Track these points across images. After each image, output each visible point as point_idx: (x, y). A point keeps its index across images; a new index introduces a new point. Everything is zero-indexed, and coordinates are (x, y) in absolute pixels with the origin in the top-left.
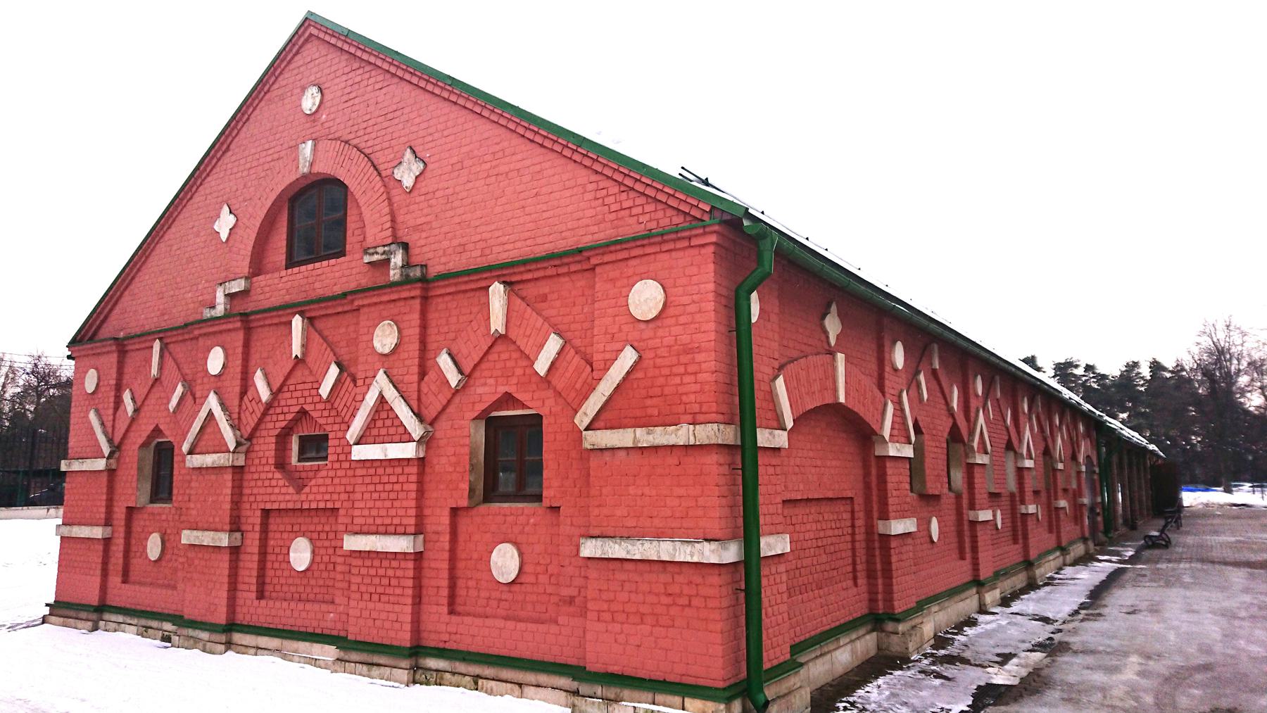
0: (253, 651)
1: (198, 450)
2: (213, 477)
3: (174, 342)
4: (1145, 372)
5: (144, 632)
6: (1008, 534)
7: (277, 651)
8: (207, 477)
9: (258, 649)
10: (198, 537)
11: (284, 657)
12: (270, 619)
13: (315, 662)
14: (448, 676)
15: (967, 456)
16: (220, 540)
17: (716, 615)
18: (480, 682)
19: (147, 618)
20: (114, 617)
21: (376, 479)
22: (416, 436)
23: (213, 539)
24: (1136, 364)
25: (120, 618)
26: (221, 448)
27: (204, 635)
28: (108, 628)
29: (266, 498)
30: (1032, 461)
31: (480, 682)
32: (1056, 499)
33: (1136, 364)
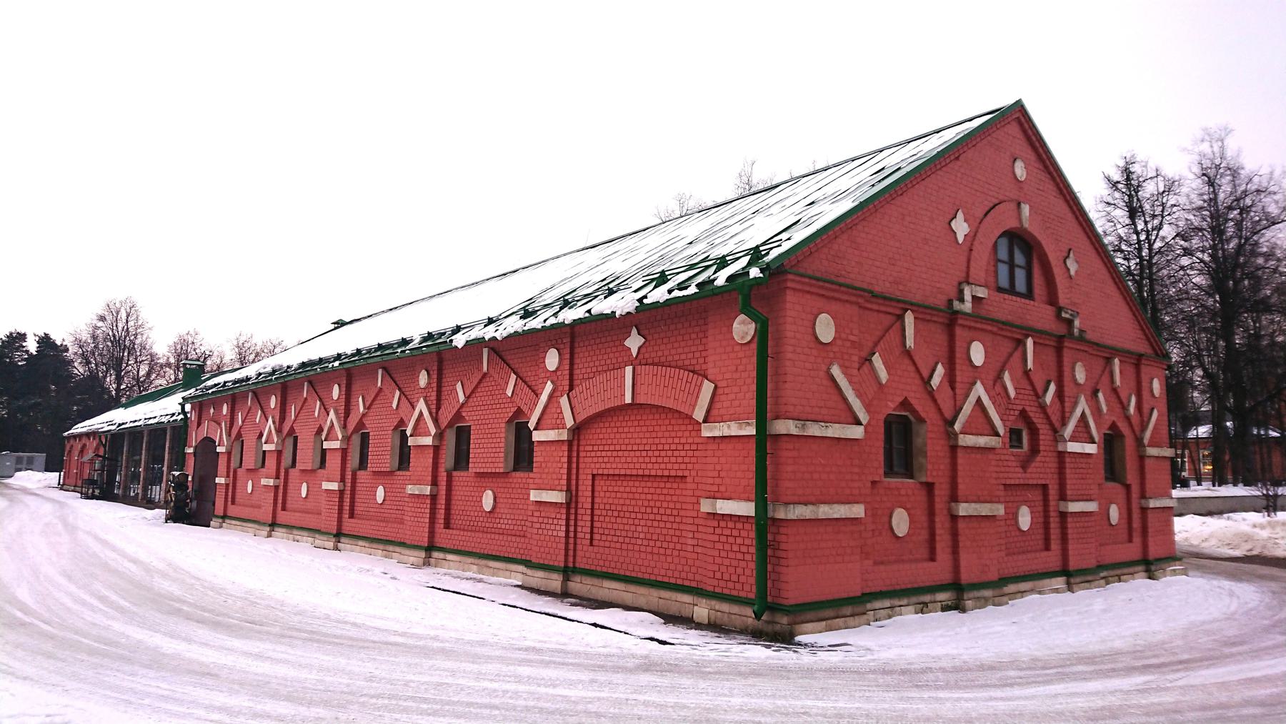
0: (1020, 595)
1: (541, 427)
2: (979, 456)
3: (794, 289)
4: (32, 346)
5: (923, 608)
6: (358, 508)
7: (1032, 591)
8: (973, 455)
9: (1022, 593)
10: (976, 509)
11: (1040, 593)
12: (1016, 570)
13: (1057, 591)
14: (1110, 579)
15: (1056, 441)
16: (998, 510)
17: (1038, 537)
18: (1122, 577)
19: (1119, 568)
20: (878, 604)
21: (647, 460)
22: (864, 422)
23: (991, 509)
24: (22, 337)
25: (887, 603)
26: (559, 425)
27: (987, 593)
28: (878, 617)
29: (1006, 475)
30: (1095, 446)
31: (1122, 577)
32: (227, 485)
33: (22, 337)
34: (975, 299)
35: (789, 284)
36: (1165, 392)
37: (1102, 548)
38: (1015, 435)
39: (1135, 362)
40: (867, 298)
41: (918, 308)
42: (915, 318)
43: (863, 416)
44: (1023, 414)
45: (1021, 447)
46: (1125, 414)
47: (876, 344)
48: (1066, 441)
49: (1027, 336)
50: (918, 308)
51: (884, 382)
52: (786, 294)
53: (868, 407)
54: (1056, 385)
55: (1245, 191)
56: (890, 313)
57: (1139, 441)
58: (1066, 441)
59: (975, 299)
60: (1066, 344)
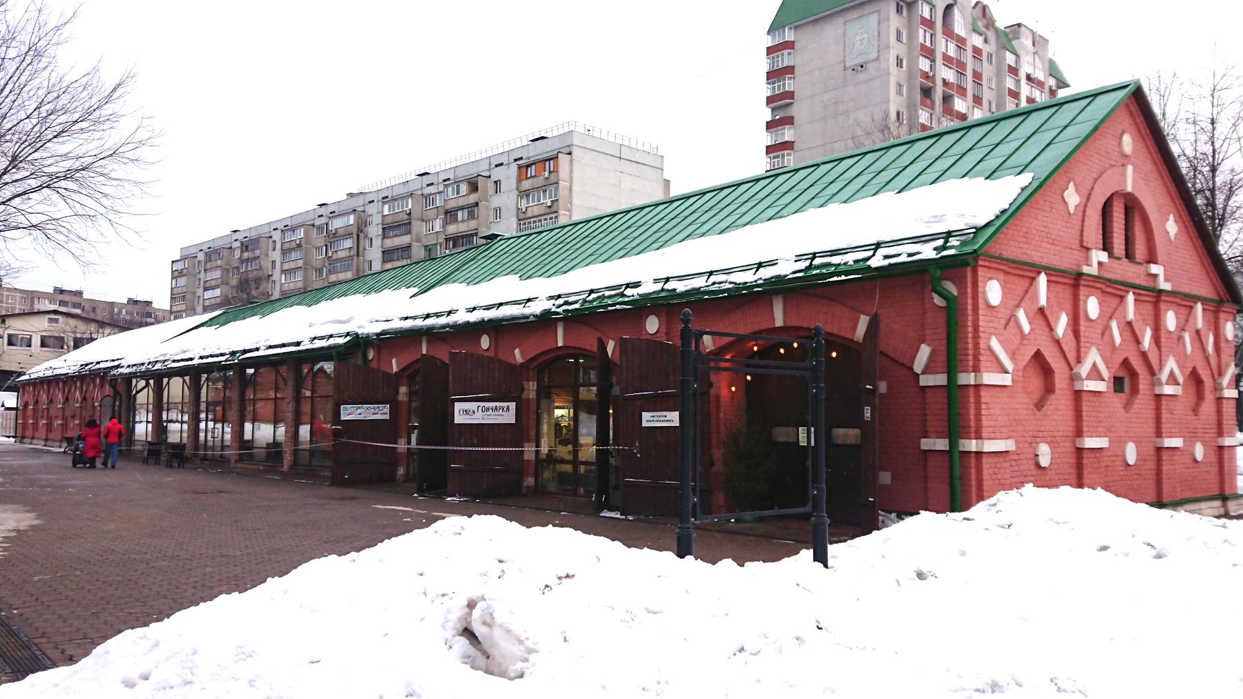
15: (1153, 385)
34: (1100, 264)
35: (1082, 282)
36: (1162, 318)
37: (522, 638)
38: (1118, 383)
39: (1072, 282)
40: (1029, 271)
41: (1051, 271)
42: (1048, 281)
43: (1009, 366)
44: (1126, 362)
45: (58, 319)
46: (1053, 337)
47: (1113, 314)
48: (1083, 380)
49: (1039, 273)
50: (1051, 271)
51: (1027, 333)
52: (1079, 289)
53: (1013, 357)
54: (1151, 330)
55: (1118, 152)
56: (1024, 276)
57: (1074, 378)
58: (1083, 380)
59: (1100, 264)
60: (980, 263)
